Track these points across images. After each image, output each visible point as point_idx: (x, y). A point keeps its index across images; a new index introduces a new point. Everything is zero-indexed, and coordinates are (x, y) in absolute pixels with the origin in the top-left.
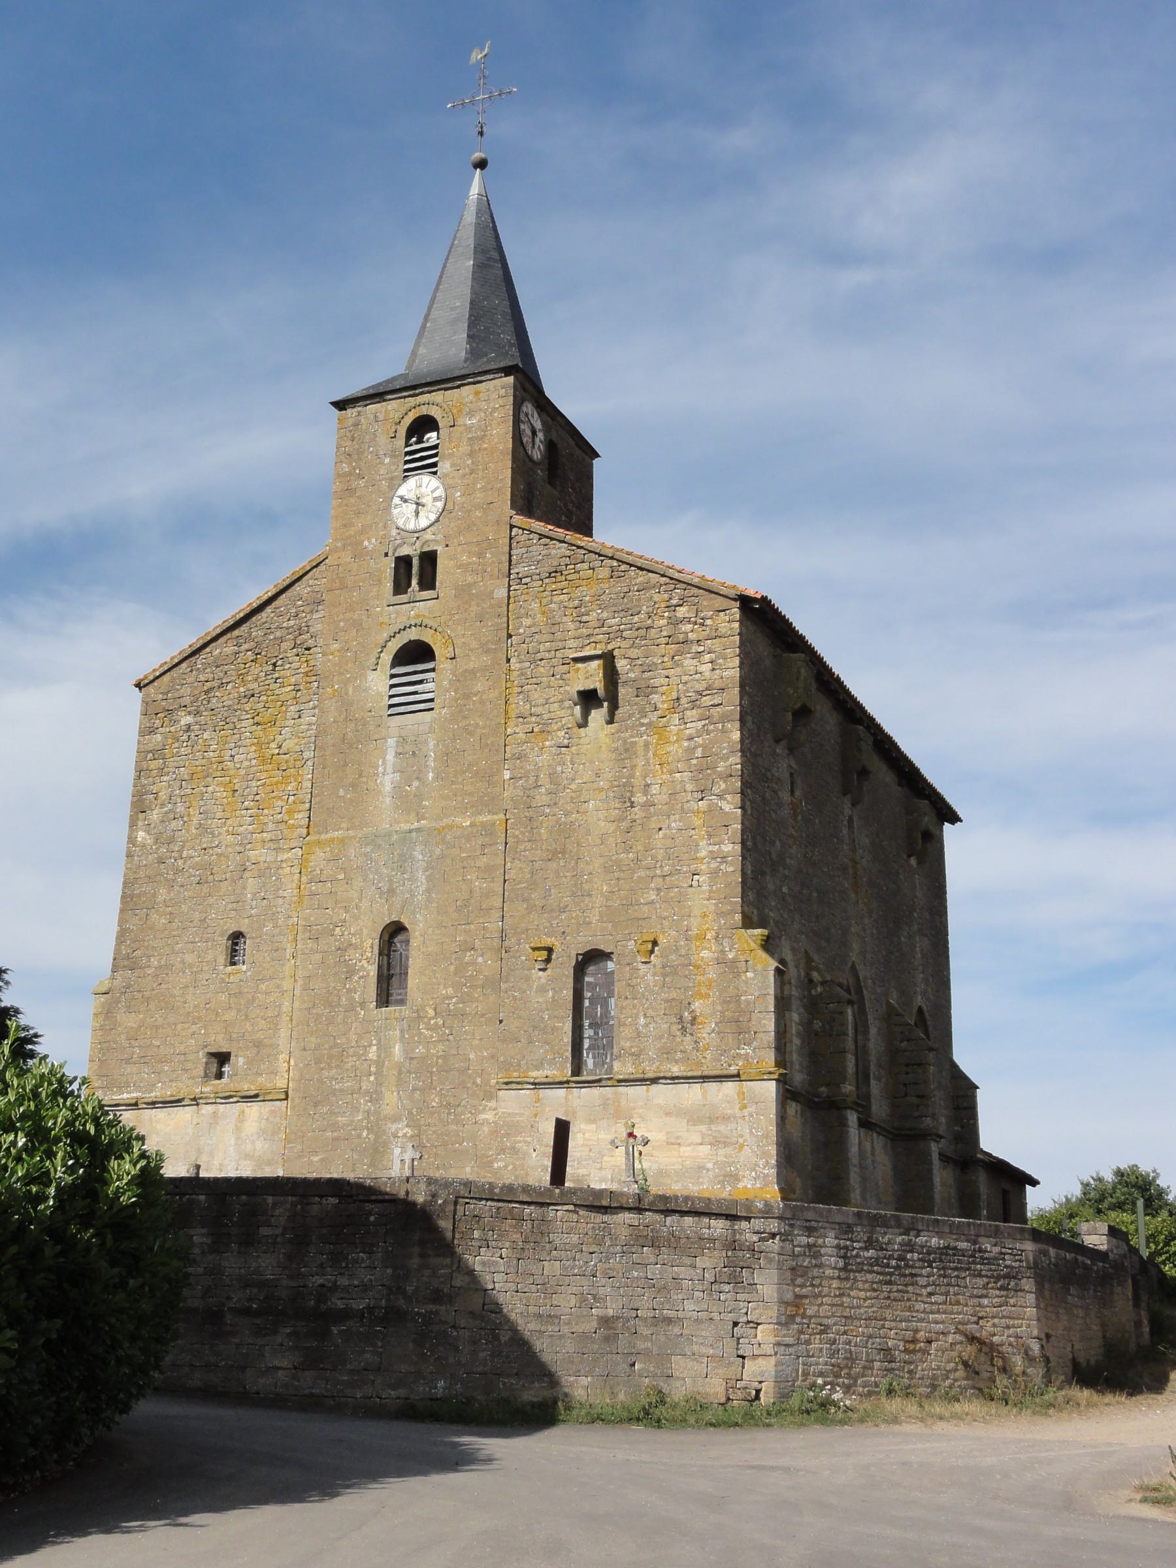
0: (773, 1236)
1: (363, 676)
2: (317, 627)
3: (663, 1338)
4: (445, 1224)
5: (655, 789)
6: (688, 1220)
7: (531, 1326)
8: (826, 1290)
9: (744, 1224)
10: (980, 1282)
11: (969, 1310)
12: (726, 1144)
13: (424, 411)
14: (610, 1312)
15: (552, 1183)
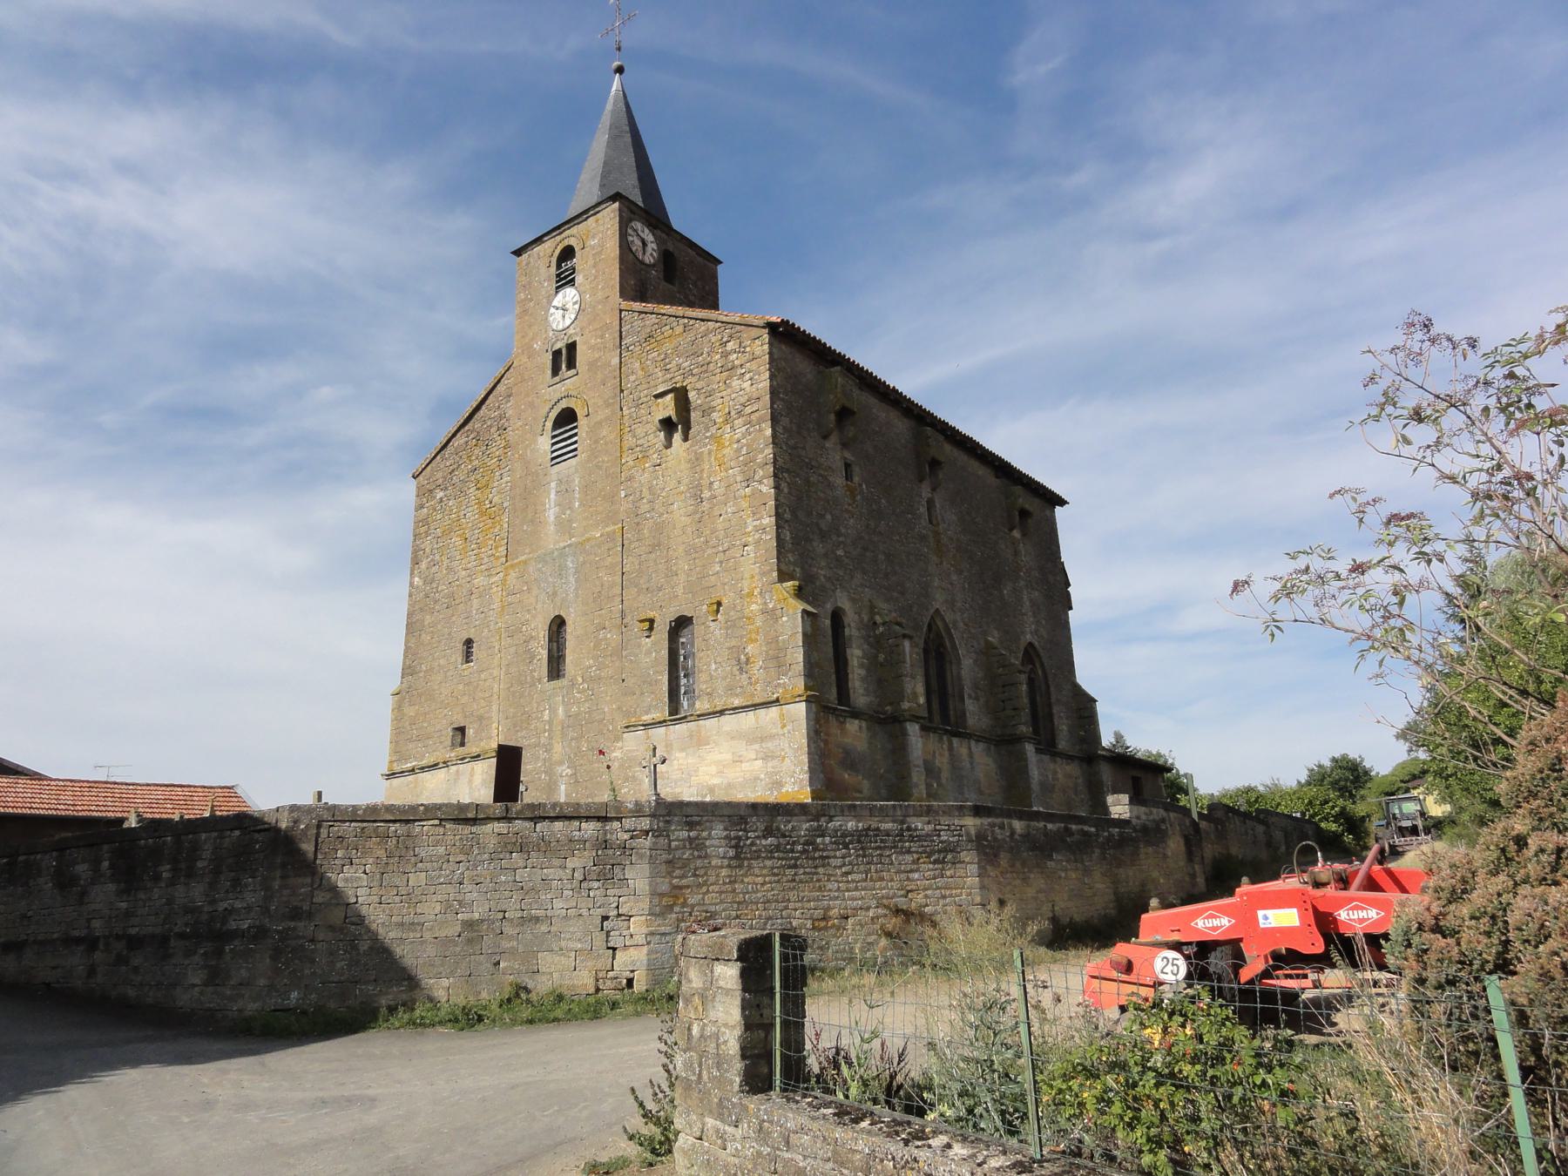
0: (647, 833)
1: (535, 442)
2: (510, 413)
3: (529, 937)
4: (307, 847)
5: (716, 485)
6: (558, 825)
7: (392, 935)
8: (712, 879)
9: (616, 824)
10: (909, 858)
11: (895, 885)
12: (773, 758)
13: (566, 243)
14: (476, 916)
15: (495, 801)
